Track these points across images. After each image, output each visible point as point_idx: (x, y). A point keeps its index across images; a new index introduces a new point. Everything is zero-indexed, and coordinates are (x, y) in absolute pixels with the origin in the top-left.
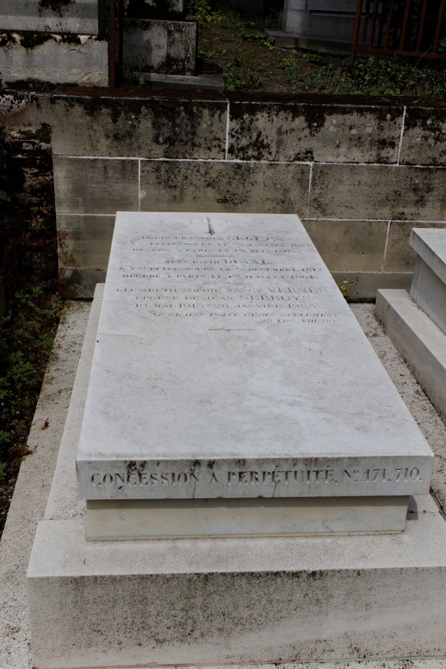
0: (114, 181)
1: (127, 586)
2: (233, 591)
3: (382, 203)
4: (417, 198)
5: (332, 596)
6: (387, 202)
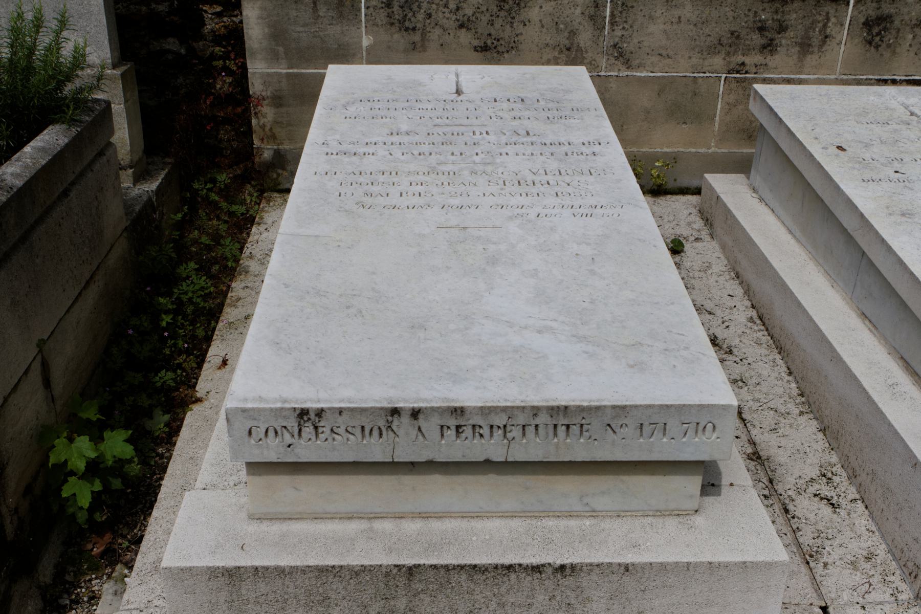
0: (327, 22)
1: (300, 580)
2: (449, 591)
3: (713, 50)
4: (763, 41)
5: (589, 599)
6: (719, 47)
